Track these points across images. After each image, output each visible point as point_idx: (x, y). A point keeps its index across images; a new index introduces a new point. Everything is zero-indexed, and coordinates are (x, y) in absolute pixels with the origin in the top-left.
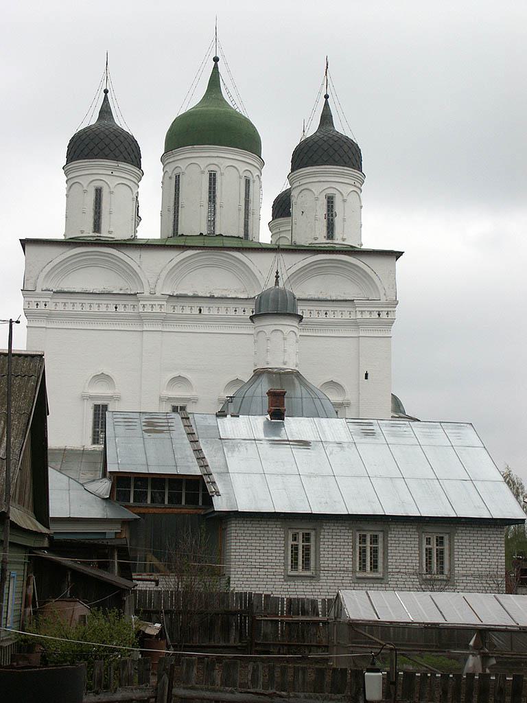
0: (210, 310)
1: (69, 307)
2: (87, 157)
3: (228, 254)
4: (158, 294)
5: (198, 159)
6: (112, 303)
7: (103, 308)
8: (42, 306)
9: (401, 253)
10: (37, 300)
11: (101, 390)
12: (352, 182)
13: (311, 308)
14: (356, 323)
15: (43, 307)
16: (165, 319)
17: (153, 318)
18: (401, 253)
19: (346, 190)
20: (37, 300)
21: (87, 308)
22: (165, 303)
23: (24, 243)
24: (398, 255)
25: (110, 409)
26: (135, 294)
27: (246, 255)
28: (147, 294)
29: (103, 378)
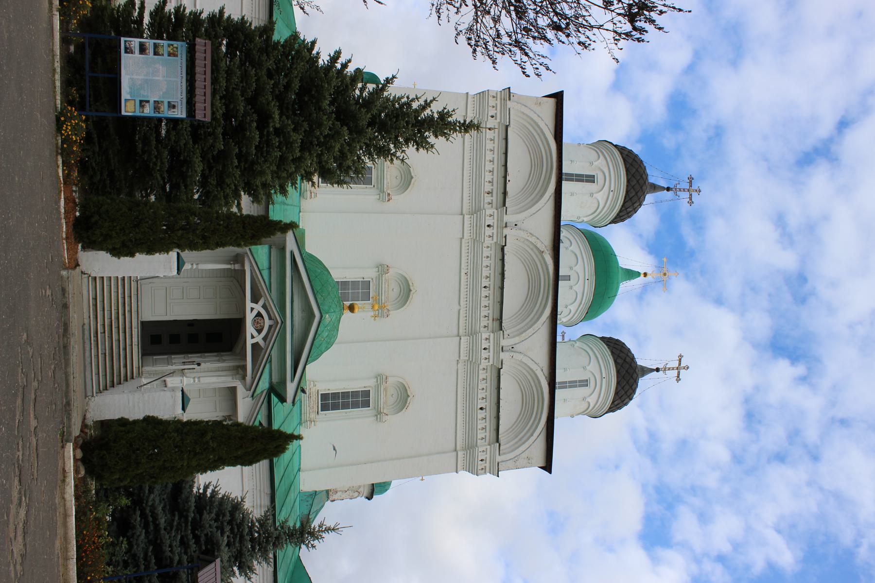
0: (486, 310)
1: (489, 166)
2: (607, 345)
3: (547, 298)
4: (506, 231)
5: (596, 361)
6: (488, 404)
7: (486, 272)
8: (485, 354)
9: (550, 472)
10: (492, 287)
11: (386, 398)
12: (604, 376)
13: (491, 297)
14: (480, 210)
15: (484, 356)
16: (472, 363)
17: (477, 229)
18: (550, 472)
19: (592, 400)
20: (488, 409)
21: (486, 262)
22: (491, 362)
23: (558, 97)
24: (548, 467)
25: (301, 442)
26: (498, 440)
27: (548, 321)
28: (506, 218)
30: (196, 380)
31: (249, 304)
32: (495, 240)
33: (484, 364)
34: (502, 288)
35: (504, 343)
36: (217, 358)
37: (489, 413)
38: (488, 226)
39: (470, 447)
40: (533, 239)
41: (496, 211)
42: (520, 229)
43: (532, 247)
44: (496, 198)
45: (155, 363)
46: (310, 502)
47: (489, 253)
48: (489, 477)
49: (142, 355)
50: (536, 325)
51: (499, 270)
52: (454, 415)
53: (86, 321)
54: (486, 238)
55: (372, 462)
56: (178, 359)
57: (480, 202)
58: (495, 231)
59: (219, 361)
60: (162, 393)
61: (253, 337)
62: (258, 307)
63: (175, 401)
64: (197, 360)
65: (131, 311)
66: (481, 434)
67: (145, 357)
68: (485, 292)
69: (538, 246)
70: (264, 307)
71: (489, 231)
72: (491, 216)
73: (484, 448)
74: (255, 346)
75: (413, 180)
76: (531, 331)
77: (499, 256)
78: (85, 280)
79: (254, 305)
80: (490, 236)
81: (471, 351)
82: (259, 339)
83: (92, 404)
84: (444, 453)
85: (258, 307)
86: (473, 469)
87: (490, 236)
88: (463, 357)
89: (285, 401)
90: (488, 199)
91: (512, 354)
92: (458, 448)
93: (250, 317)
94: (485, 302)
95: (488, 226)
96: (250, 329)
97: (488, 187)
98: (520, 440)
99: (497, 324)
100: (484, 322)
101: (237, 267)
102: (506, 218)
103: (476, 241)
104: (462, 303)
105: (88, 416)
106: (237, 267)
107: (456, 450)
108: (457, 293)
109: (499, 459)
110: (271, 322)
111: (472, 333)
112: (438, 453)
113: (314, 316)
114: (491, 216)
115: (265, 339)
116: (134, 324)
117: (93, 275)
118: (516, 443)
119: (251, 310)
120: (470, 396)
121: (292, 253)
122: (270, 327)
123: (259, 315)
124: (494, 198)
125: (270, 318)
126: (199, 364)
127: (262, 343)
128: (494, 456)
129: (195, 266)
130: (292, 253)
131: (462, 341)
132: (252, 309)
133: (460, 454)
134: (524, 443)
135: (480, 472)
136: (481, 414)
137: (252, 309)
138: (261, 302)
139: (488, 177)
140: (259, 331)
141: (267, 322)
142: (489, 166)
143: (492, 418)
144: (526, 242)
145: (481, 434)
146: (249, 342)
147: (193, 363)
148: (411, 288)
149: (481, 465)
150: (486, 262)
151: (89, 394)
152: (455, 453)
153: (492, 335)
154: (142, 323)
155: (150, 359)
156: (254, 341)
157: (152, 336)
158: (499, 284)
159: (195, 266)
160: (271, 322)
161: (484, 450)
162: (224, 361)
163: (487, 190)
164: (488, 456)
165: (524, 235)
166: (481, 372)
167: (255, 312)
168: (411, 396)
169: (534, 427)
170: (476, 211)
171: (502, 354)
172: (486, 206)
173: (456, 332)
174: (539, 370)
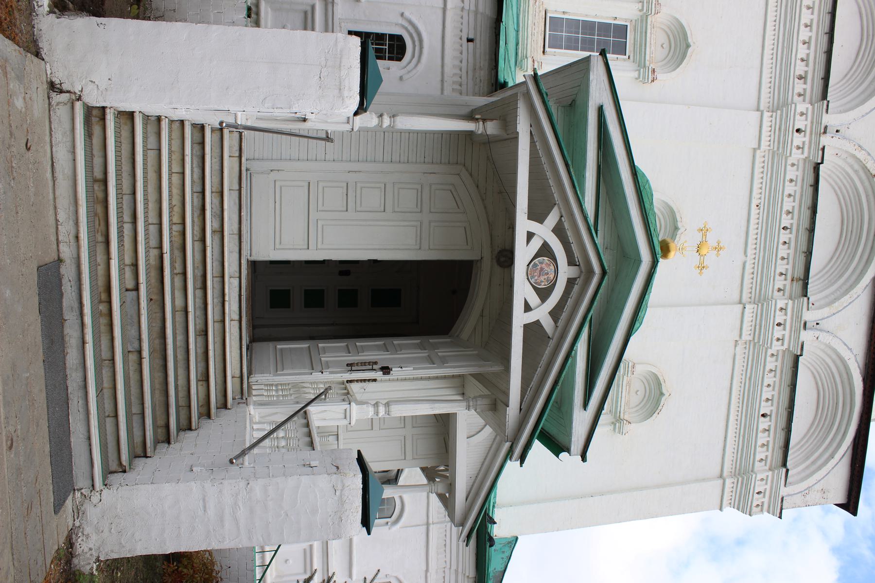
0: (785, 263)
4: (825, 140)
7: (788, 205)
8: (778, 332)
9: (854, 513)
13: (793, 244)
16: (757, 345)
17: (782, 134)
18: (854, 513)
21: (790, 188)
24: (851, 505)
26: (784, 464)
28: (827, 119)
29: (680, 46)
30: (382, 410)
31: (523, 224)
32: (806, 154)
33: (777, 347)
34: (811, 230)
35: (809, 316)
36: (424, 354)
37: (775, 423)
38: (798, 131)
39: (743, 473)
40: (861, 155)
41: (810, 107)
42: (845, 138)
43: (856, 167)
44: (813, 85)
45: (280, 366)
46: (507, 554)
47: (796, 173)
48: (766, 519)
49: (253, 339)
50: (855, 290)
51: (808, 201)
52: (723, 423)
53: (67, 252)
54: (794, 150)
55: (602, 494)
56: (334, 352)
57: (786, 91)
58: (807, 139)
59: (431, 361)
60: (305, 479)
61: (528, 308)
62: (544, 232)
63: (341, 502)
64: (382, 357)
65: (220, 232)
66: (761, 454)
67: (256, 345)
68: (784, 236)
69: (869, 166)
70: (559, 231)
71: (798, 139)
72: (802, 114)
73: (763, 476)
74: (533, 330)
75: (690, 50)
76: (846, 299)
77: (811, 180)
78: (62, 113)
79: (534, 226)
80: (798, 148)
81: (759, 327)
82: (542, 313)
83: (92, 512)
84: (704, 480)
85: (544, 232)
86: (744, 505)
87: (798, 148)
88: (746, 337)
89: (568, 450)
90: (799, 87)
91: (817, 333)
92: (725, 474)
93: (523, 253)
94: (783, 251)
95: (798, 131)
96: (523, 291)
97: (800, 68)
98: (813, 463)
99: (798, 286)
100: (780, 283)
101: (491, 128)
102: (827, 119)
103: (778, 154)
104: (750, 252)
105: (82, 546)
106: (491, 128)
107: (721, 476)
108: (743, 235)
109: (784, 491)
110: (572, 272)
111: (761, 300)
112: (697, 480)
113: (639, 261)
114: (802, 114)
115: (555, 314)
116: (231, 267)
117: (94, 99)
118: (807, 467)
119: (530, 235)
120: (749, 397)
121: (600, 110)
122: (571, 282)
123: (545, 250)
124: (808, 87)
125: (571, 262)
126: (386, 370)
127: (548, 324)
128: (778, 489)
129: (386, 121)
130: (600, 110)
131: (746, 310)
132: (530, 236)
133: (729, 482)
134: (820, 468)
135: (754, 509)
136: (764, 423)
137: (530, 236)
138: (552, 219)
139: (802, 51)
140: (544, 294)
141: (565, 271)
142: (804, 34)
143: (779, 430)
144: (850, 160)
145: (761, 454)
146: (519, 319)
147: (370, 365)
148: (679, 225)
149: (757, 500)
150: (790, 188)
151: (81, 482)
152: (720, 481)
153: (790, 302)
154: (254, 265)
155: (267, 350)
156: (531, 317)
157: (272, 292)
158: (806, 223)
159: (386, 121)
160: (572, 272)
161: (763, 477)
162: (443, 361)
163: (797, 73)
164: (768, 487)
165: (851, 149)
166: (769, 359)
167: (536, 244)
168: (667, 395)
169: (835, 445)
170: (781, 106)
171: (803, 332)
172: (796, 98)
173: (736, 297)
174: (852, 357)
